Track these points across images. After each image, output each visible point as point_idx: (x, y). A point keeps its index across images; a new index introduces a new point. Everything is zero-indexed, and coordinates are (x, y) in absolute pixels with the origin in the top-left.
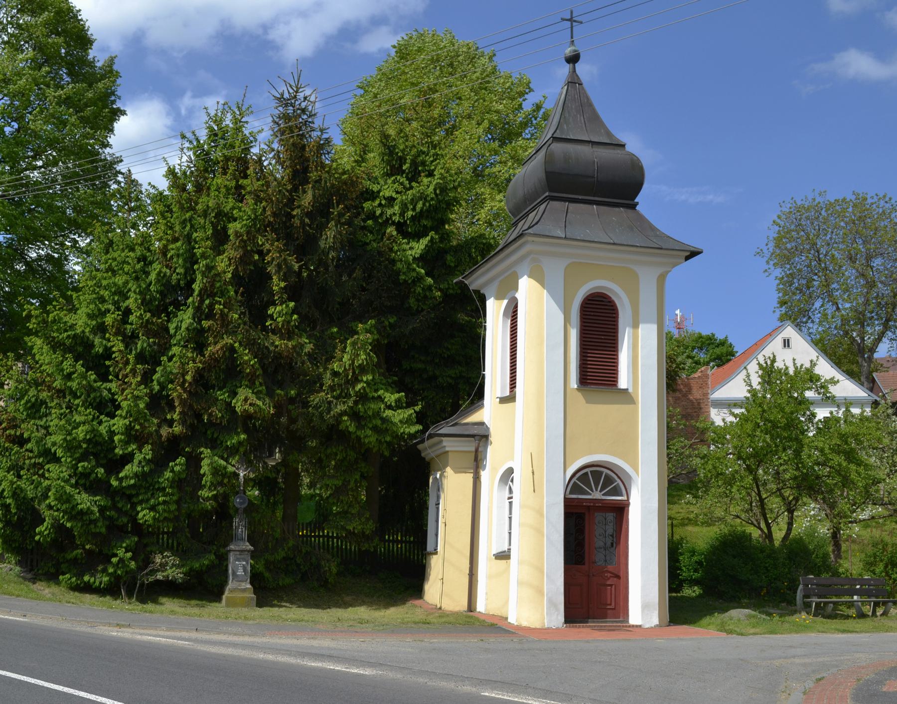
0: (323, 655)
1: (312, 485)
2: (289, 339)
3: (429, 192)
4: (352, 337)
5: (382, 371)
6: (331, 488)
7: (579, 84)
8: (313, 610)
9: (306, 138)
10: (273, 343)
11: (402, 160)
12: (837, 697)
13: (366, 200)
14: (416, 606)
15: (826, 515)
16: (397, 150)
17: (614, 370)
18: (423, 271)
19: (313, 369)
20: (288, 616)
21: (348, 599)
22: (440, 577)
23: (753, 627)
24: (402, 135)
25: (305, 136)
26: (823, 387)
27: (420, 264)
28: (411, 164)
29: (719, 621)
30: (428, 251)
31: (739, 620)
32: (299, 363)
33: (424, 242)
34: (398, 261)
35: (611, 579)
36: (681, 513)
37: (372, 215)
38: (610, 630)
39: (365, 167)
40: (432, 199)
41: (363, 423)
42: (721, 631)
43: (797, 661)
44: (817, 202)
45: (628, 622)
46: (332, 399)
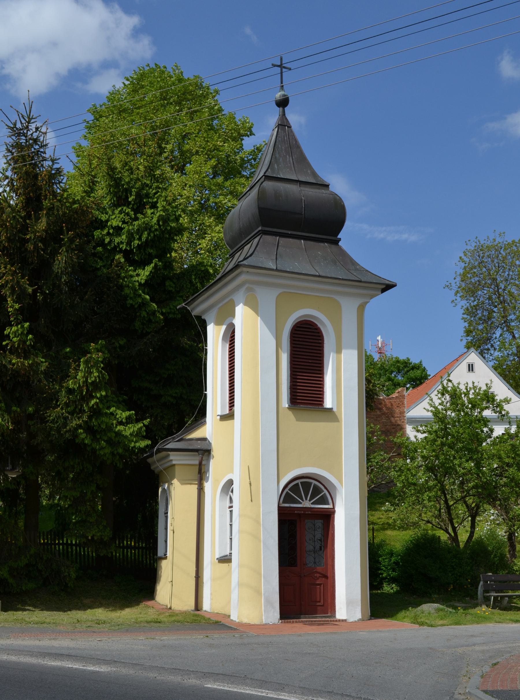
0: (62, 655)
1: (51, 496)
2: (26, 358)
3: (153, 223)
4: (86, 356)
5: (114, 389)
6: (70, 499)
7: (288, 127)
8: (55, 612)
9: (39, 168)
10: (10, 362)
11: (128, 191)
12: (509, 680)
13: (97, 228)
14: (148, 607)
15: (503, 519)
16: (123, 183)
17: (320, 391)
18: (148, 297)
19: (49, 387)
20: (31, 619)
21: (86, 601)
22: (170, 580)
23: (442, 619)
24: (127, 168)
25: (38, 165)
26: (498, 407)
27: (146, 290)
28: (136, 196)
29: (413, 615)
30: (153, 277)
31: (429, 613)
32: (35, 382)
33: (149, 269)
34: (126, 287)
35: (320, 579)
36: (382, 518)
37: (101, 243)
38: (319, 625)
39: (94, 197)
40: (156, 230)
41: (98, 437)
42: (414, 623)
43: (477, 648)
44: (497, 242)
45: (335, 617)
46: (67, 415)
